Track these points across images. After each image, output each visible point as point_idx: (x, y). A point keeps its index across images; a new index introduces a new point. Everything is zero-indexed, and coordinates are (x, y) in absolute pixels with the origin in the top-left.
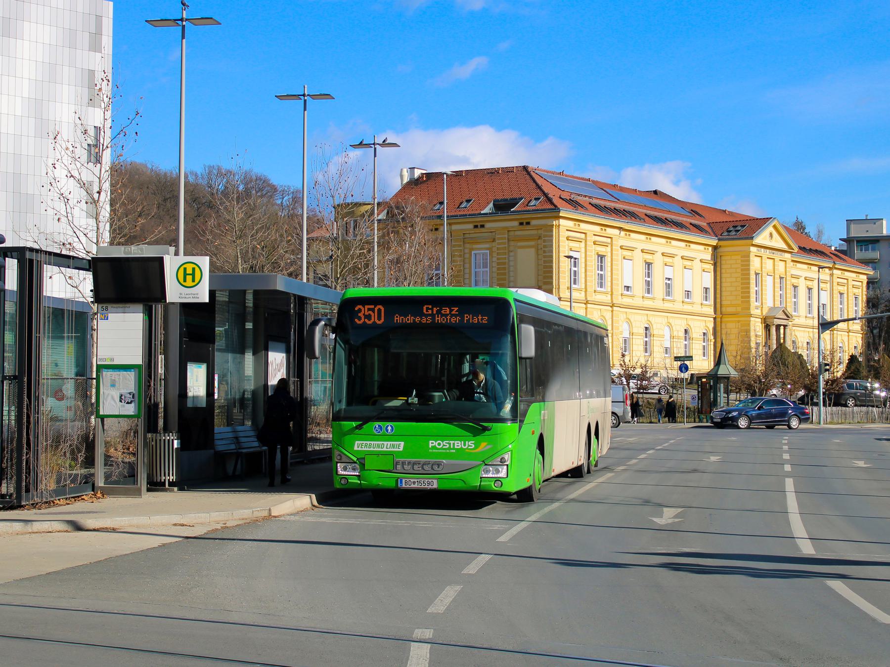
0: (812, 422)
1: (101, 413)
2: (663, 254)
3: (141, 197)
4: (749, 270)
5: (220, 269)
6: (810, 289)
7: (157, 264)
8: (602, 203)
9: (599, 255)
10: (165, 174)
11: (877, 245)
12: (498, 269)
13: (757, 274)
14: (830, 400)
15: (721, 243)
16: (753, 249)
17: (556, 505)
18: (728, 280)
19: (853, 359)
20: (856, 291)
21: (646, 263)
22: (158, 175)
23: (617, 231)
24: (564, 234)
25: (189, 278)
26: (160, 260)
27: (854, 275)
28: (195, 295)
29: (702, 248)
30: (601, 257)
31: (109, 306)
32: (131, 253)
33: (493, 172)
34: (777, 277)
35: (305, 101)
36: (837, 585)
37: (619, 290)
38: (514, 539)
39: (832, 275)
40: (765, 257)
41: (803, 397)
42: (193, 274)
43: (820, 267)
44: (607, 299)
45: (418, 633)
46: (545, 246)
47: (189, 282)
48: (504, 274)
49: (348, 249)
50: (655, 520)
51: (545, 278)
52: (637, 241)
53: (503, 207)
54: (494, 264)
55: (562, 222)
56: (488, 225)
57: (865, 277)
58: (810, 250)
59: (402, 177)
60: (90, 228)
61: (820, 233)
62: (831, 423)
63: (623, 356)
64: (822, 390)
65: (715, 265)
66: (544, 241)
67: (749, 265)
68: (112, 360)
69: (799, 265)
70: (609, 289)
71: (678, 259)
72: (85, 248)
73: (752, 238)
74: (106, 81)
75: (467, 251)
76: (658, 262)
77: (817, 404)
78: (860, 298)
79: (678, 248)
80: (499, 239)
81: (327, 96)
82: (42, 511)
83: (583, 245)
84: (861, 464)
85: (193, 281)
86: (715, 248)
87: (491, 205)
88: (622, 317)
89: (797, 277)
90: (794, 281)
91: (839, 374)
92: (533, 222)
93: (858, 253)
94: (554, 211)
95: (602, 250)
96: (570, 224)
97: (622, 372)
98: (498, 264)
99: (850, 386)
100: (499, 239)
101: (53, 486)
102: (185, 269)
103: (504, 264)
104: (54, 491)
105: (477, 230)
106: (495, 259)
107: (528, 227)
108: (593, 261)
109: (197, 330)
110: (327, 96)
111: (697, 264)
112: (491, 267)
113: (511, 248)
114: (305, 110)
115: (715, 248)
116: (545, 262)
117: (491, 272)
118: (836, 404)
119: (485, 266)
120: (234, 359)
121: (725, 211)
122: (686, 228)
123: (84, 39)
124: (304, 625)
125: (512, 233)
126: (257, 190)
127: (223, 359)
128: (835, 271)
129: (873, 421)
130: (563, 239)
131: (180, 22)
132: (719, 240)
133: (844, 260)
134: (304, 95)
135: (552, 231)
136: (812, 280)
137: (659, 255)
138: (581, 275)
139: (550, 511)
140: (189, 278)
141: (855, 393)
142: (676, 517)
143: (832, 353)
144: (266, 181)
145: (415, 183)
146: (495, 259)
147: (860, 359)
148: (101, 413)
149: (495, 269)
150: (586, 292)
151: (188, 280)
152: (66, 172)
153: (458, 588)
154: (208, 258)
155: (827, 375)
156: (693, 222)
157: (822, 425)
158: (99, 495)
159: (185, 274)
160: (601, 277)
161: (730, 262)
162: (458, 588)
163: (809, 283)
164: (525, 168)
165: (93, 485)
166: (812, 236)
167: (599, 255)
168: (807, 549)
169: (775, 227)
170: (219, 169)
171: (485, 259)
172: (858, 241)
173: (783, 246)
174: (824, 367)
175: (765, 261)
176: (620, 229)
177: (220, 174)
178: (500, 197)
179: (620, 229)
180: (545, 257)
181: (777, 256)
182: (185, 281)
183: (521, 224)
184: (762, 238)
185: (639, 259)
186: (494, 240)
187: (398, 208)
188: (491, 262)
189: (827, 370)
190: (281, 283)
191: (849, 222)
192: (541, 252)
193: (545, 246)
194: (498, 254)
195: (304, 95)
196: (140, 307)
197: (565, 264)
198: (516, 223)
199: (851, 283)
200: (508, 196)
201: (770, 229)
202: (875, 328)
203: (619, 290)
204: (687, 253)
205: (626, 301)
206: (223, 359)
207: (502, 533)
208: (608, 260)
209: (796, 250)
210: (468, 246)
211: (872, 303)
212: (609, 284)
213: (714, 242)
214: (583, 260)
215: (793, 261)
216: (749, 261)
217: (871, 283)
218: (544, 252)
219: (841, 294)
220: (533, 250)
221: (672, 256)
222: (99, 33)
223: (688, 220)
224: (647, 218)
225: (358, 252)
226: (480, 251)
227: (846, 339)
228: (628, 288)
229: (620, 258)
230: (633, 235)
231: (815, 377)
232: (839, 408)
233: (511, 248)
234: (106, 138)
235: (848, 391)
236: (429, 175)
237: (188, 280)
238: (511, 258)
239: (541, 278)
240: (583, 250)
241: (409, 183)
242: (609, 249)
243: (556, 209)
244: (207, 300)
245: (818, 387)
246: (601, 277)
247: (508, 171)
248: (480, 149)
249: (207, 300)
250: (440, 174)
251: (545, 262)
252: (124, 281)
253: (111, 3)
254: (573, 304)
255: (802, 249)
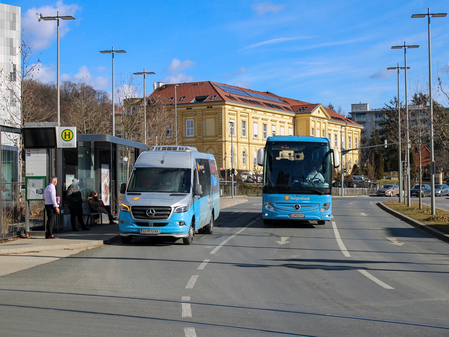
0: (338, 195)
1: (28, 198)
2: (262, 119)
3: (37, 97)
4: (309, 127)
5: (80, 133)
6: (336, 135)
7: (52, 130)
8: (244, 98)
9: (243, 121)
10: (45, 85)
11: (364, 116)
12: (198, 128)
13: (313, 129)
14: (346, 185)
15: (297, 115)
16: (311, 118)
17: (232, 237)
18: (300, 132)
19: (355, 166)
20: (356, 136)
21: (264, 124)
22: (41, 86)
23: (251, 110)
24: (227, 112)
25: (67, 137)
26: (54, 129)
27: (355, 129)
28: (70, 145)
29: (288, 117)
30: (244, 122)
31: (31, 150)
32: (40, 126)
33: (195, 84)
34: (322, 130)
35: (113, 54)
36: (363, 272)
37: (252, 137)
38: (217, 252)
39: (345, 129)
40: (316, 121)
41: (334, 183)
42: (69, 135)
43: (342, 126)
44: (247, 141)
45: (184, 298)
46: (219, 117)
47: (67, 138)
48: (201, 130)
49: (133, 120)
50: (278, 242)
51: (219, 131)
52: (260, 115)
53: (200, 100)
54: (196, 126)
55: (226, 106)
56: (193, 108)
57: (360, 130)
58: (336, 118)
59: (154, 86)
60: (18, 113)
61: (340, 110)
62: (347, 195)
63: (255, 166)
64: (343, 181)
65: (294, 125)
66: (219, 115)
67: (309, 125)
68: (33, 174)
69: (331, 125)
70: (248, 136)
71: (278, 123)
72: (18, 122)
73: (310, 113)
74: (24, 46)
75: (184, 120)
76: (269, 123)
77: (340, 187)
78: (358, 139)
79: (278, 118)
80: (198, 114)
81: (123, 51)
82: (3, 244)
83: (236, 116)
84: (363, 214)
85: (69, 138)
86: (294, 117)
87: (194, 99)
88: (253, 148)
89: (330, 130)
90: (329, 132)
91: (350, 173)
92: (214, 107)
93: (356, 119)
94: (223, 102)
95: (244, 119)
96: (230, 107)
97: (254, 173)
98: (198, 125)
99: (355, 178)
100: (198, 114)
101: (7, 232)
102: (65, 133)
103: (201, 125)
104: (8, 234)
105: (188, 110)
106: (196, 123)
107: (211, 109)
108: (240, 124)
109: (70, 160)
110: (123, 51)
111: (286, 125)
112: (195, 127)
113: (204, 118)
114: (113, 57)
115: (294, 117)
116: (219, 124)
117: (195, 129)
118: (349, 187)
119: (192, 127)
120: (86, 172)
121: (298, 101)
122: (282, 109)
123: (7, 24)
124: (132, 295)
125: (204, 112)
126: (88, 92)
127: (81, 172)
128: (347, 127)
129: (365, 194)
130: (227, 114)
131: (56, 18)
132: (296, 114)
133: (351, 122)
134: (112, 51)
135: (222, 110)
136: (337, 131)
137: (269, 121)
138: (235, 130)
139: (231, 239)
140: (67, 137)
141: (357, 182)
142: (287, 241)
143: (346, 164)
144: (91, 89)
145: (160, 89)
146: (196, 123)
147: (358, 166)
148: (28, 198)
149: (196, 128)
150: (237, 138)
151: (67, 137)
152: (6, 88)
153: (197, 276)
154: (76, 128)
155: (345, 174)
156: (284, 106)
157: (343, 196)
158: (28, 236)
159: (66, 135)
160: (244, 131)
161: (301, 125)
162: (197, 276)
163: (336, 133)
164: (209, 82)
165: (25, 231)
166: (336, 111)
167: (243, 121)
168: (347, 255)
169: (320, 108)
170: (70, 83)
171: (192, 123)
172: (356, 114)
173: (324, 116)
174: (345, 170)
175: (322, 124)
176: (252, 109)
177: (70, 85)
178: (198, 95)
179: (252, 109)
180: (219, 122)
181: (322, 121)
182: (65, 138)
183: (208, 107)
184: (315, 113)
185: (261, 122)
186: (196, 115)
187: (152, 101)
188: (195, 125)
189: (345, 172)
190: (108, 139)
191: (353, 105)
192: (217, 120)
193: (219, 117)
194: (198, 121)
195: (112, 51)
196: (45, 150)
197: (228, 126)
198: (206, 107)
199: (354, 132)
200: (202, 95)
201: (318, 109)
202: (364, 152)
203: (252, 137)
204: (264, 117)
205: (255, 141)
206: (81, 172)
207: (212, 250)
208: (247, 123)
209: (330, 118)
210: (184, 117)
211: (363, 141)
212: (248, 134)
213: (294, 115)
214: (236, 124)
215: (329, 123)
216: (309, 123)
217: (363, 132)
218: (219, 120)
219: (350, 137)
220: (214, 119)
221: (275, 121)
222: (14, 21)
223: (263, 101)
224: (284, 108)
225: (138, 122)
226: (190, 119)
227: (352, 157)
228: (256, 136)
229: (252, 122)
230: (258, 112)
231: (339, 175)
232: (350, 188)
233: (204, 118)
234: (18, 68)
235: (354, 180)
236: (166, 86)
237: (67, 137)
238: (204, 123)
239: (217, 131)
240: (236, 119)
241: (157, 89)
242: (247, 118)
243: (224, 101)
244: (76, 147)
245: (341, 179)
246: (244, 131)
247: (202, 83)
248: (179, 72)
249: (76, 147)
250: (173, 85)
251: (219, 124)
252: (37, 139)
253: (20, 8)
254: (233, 143)
255: (332, 117)
